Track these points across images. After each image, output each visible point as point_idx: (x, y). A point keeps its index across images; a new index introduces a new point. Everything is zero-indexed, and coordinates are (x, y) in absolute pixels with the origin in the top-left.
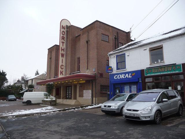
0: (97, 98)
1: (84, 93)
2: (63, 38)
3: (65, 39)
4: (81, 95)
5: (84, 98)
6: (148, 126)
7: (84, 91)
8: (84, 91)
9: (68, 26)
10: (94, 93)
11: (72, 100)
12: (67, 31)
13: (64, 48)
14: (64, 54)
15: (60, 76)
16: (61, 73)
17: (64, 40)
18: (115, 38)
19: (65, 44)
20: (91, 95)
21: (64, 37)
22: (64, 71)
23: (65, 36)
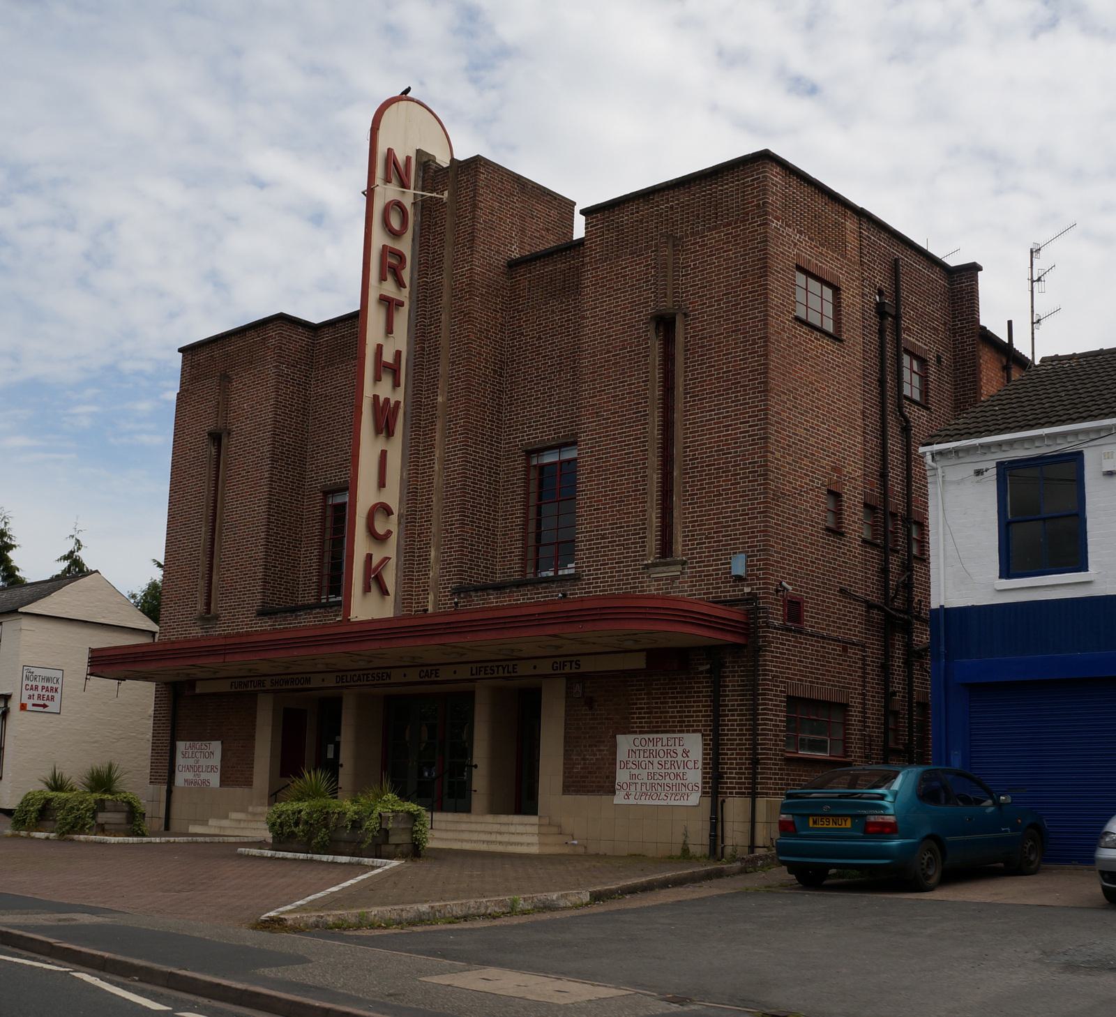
0: (761, 803)
1: (622, 755)
2: (394, 261)
3: (406, 275)
4: (593, 778)
5: (619, 799)
6: (196, 934)
7: (625, 743)
8: (625, 743)
9: (431, 159)
10: (734, 761)
11: (473, 818)
12: (425, 207)
13: (398, 354)
14: (397, 403)
15: (365, 607)
16: (374, 579)
17: (400, 283)
18: (881, 310)
19: (402, 320)
20: (695, 776)
21: (401, 257)
22: (392, 563)
23: (405, 246)
